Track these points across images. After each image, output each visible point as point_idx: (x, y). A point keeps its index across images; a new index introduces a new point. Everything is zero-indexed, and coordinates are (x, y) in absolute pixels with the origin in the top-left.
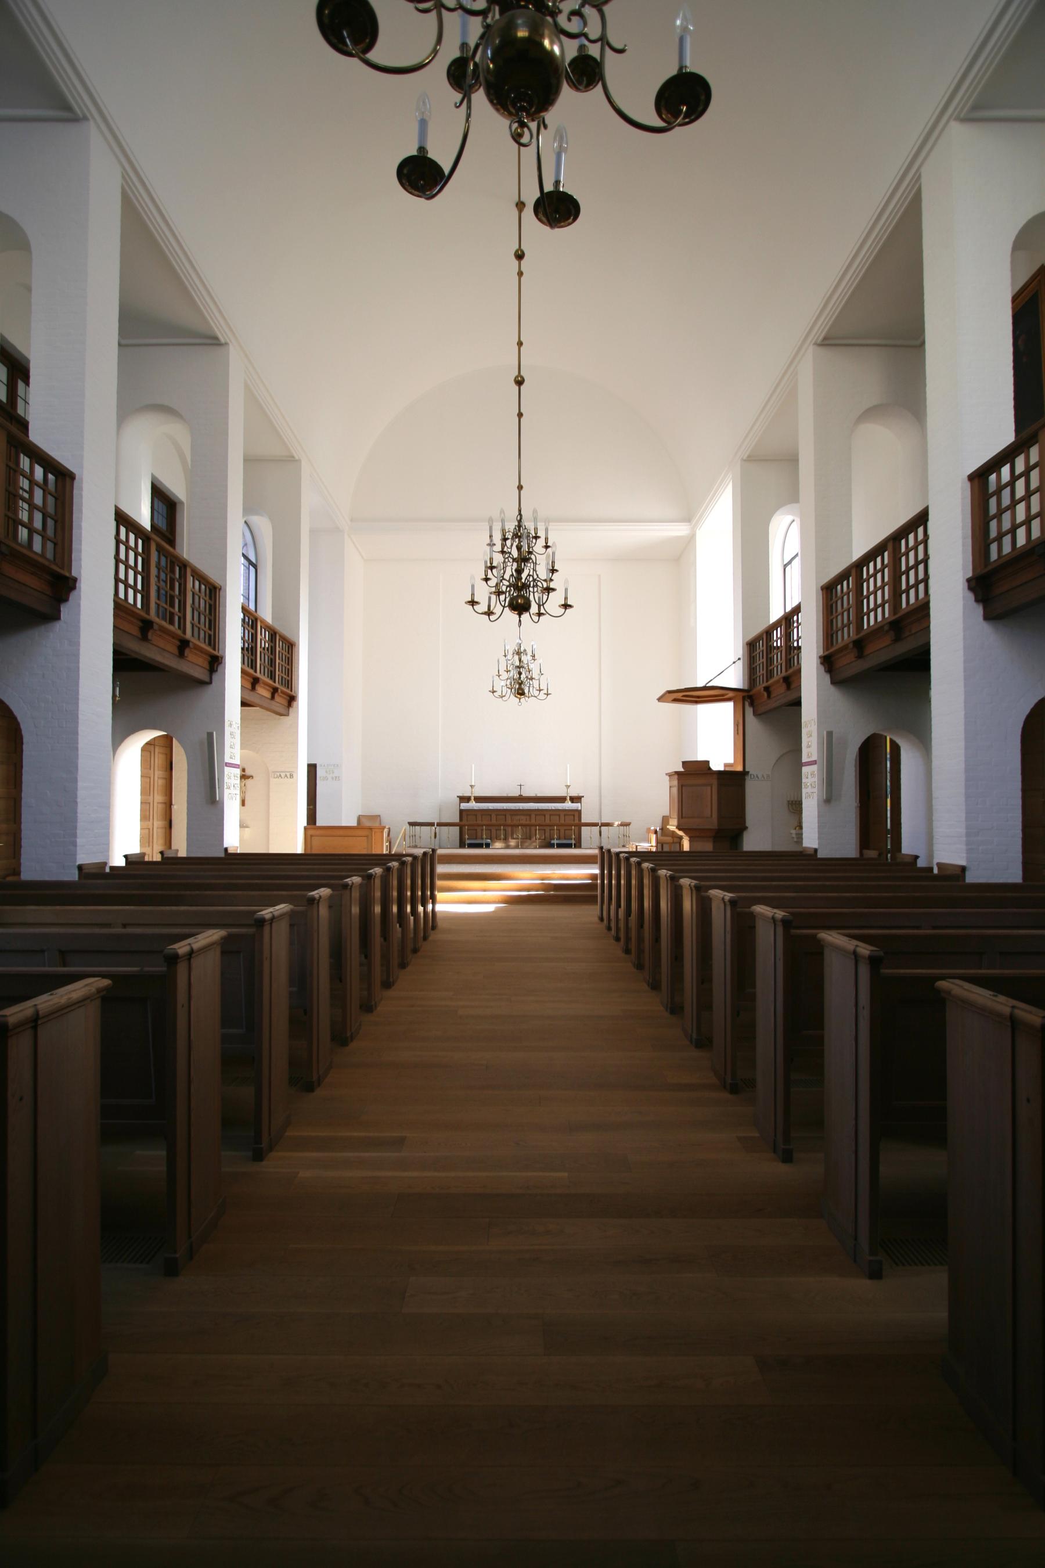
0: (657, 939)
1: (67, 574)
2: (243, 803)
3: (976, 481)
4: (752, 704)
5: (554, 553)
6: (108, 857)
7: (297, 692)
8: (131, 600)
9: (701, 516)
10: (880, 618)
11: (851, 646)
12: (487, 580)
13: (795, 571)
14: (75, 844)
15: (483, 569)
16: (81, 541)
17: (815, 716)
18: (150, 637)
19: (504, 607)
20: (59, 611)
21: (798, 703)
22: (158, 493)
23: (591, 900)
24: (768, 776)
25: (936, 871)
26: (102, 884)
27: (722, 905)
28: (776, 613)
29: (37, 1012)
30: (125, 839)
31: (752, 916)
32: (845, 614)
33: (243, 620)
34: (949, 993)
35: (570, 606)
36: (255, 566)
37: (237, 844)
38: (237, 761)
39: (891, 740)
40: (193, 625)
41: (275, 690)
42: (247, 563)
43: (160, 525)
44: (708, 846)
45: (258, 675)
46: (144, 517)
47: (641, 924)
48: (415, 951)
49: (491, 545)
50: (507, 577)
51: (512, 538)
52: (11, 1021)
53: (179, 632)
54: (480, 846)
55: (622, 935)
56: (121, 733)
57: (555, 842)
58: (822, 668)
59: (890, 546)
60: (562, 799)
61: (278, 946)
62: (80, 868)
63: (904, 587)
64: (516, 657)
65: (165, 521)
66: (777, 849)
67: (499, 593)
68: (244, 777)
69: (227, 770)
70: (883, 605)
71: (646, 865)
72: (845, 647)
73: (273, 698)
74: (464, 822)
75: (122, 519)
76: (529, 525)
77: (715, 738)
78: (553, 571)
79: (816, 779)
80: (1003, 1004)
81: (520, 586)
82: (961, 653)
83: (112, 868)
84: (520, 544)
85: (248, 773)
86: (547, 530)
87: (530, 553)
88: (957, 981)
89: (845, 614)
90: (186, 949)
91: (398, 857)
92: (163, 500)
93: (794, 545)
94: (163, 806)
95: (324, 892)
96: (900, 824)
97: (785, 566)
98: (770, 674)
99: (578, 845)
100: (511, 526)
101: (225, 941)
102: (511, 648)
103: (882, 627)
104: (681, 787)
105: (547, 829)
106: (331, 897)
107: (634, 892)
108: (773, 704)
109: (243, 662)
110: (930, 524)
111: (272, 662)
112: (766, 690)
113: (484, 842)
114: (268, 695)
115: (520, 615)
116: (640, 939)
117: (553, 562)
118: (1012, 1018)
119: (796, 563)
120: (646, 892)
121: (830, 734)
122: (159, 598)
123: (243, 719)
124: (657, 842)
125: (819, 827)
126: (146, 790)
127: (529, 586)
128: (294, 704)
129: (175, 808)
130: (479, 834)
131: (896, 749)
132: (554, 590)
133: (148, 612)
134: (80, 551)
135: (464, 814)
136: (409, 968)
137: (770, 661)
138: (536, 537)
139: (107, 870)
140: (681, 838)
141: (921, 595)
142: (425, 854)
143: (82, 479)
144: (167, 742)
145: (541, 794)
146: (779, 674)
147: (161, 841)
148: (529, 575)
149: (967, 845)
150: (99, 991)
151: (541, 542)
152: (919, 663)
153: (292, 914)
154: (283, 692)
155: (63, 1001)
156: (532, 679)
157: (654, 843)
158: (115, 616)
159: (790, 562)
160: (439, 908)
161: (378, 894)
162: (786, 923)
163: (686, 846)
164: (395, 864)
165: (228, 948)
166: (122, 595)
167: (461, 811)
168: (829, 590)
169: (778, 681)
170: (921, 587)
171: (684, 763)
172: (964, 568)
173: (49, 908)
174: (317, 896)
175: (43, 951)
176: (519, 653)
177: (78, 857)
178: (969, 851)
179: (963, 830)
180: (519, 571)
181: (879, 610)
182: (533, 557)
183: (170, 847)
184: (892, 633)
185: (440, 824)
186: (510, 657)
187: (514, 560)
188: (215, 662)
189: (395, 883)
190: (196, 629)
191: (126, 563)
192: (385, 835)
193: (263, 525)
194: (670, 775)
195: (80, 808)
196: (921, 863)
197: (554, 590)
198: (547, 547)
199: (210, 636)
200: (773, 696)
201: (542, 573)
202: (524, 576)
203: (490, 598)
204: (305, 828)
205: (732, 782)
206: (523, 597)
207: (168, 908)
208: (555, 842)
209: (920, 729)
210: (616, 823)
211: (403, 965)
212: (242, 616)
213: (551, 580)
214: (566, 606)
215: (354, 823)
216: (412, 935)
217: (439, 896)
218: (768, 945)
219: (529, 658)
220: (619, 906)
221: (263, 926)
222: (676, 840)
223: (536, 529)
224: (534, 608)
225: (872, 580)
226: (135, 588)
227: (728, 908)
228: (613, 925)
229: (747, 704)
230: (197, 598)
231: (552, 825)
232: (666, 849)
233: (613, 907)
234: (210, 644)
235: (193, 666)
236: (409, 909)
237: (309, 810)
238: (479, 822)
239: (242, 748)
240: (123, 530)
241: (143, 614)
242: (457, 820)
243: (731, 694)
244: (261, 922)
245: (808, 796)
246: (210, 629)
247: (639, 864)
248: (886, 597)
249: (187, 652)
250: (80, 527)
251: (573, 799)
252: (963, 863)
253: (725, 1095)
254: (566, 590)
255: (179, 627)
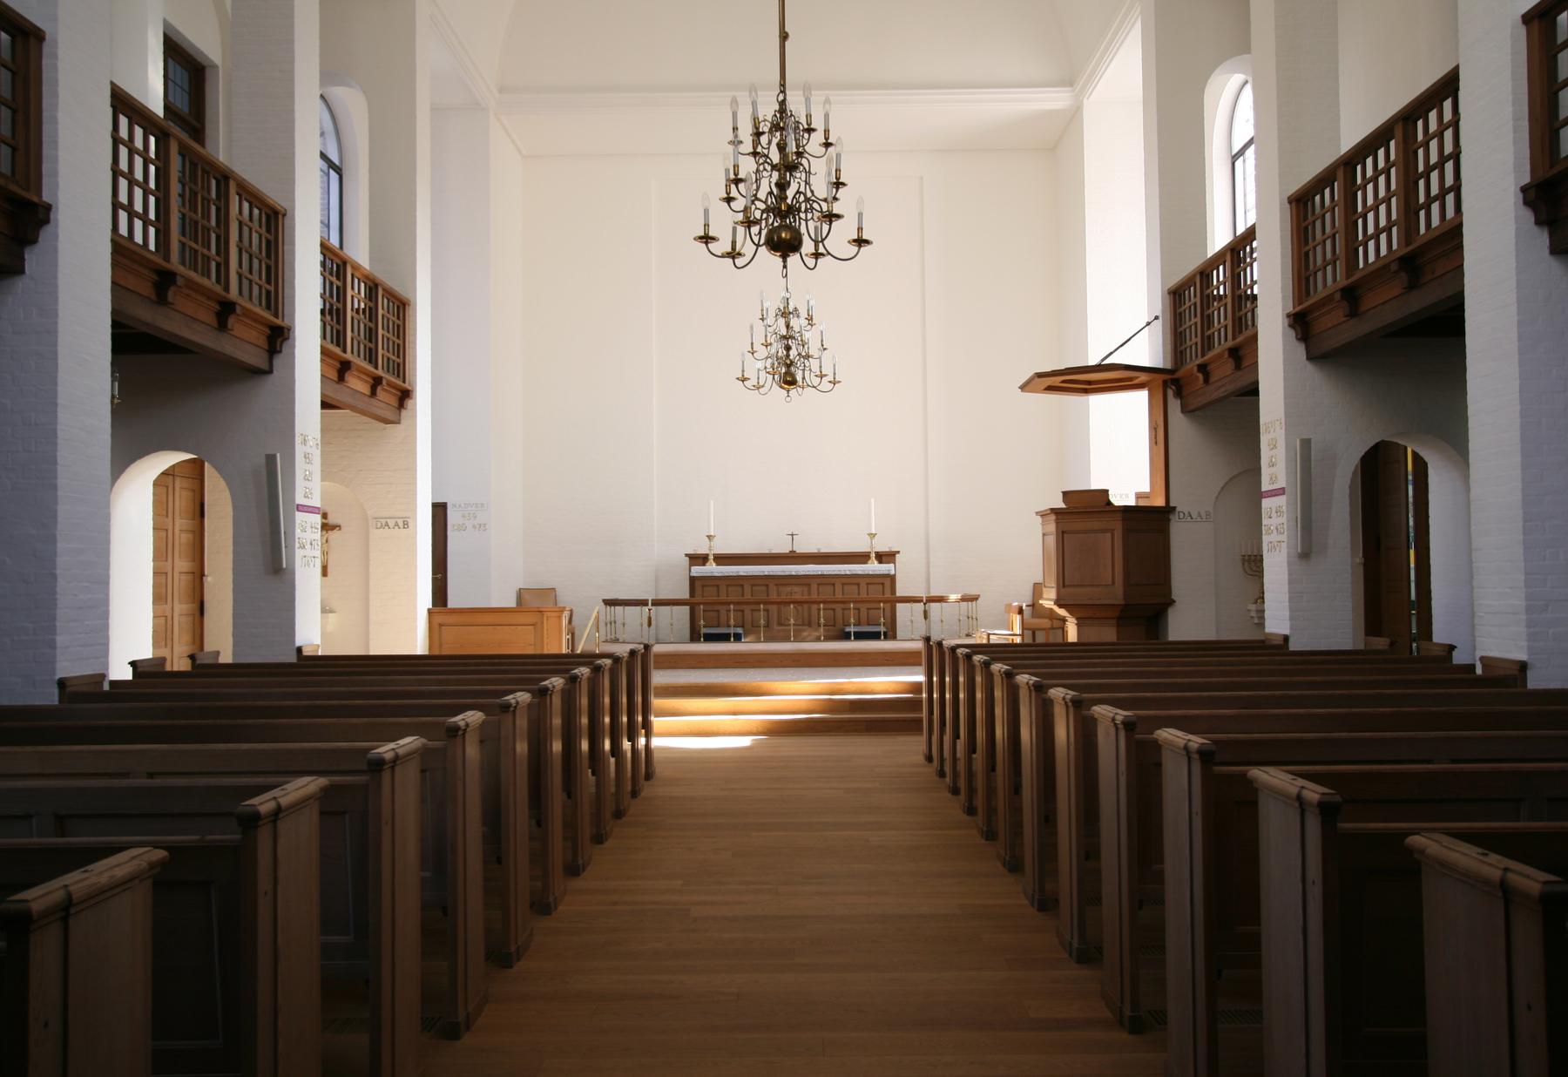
0: (1017, 789)
1: (35, 199)
2: (325, 573)
3: (1536, 23)
4: (1178, 394)
5: (838, 156)
6: (106, 665)
7: (414, 383)
8: (138, 238)
9: (1093, 73)
10: (1384, 251)
11: (1338, 296)
12: (729, 200)
13: (1248, 166)
14: (52, 645)
15: (724, 182)
16: (56, 143)
17: (1281, 413)
18: (170, 299)
19: (758, 245)
20: (23, 259)
21: (1253, 391)
22: (175, 51)
23: (912, 727)
24: (1208, 514)
25: (1479, 671)
26: (94, 709)
27: (1113, 730)
28: (1219, 238)
29: (69, 895)
30: (131, 638)
31: (1156, 746)
32: (1328, 242)
33: (323, 264)
34: (1422, 852)
35: (867, 242)
36: (339, 170)
37: (318, 641)
38: (316, 502)
39: (1415, 454)
40: (240, 276)
41: (376, 382)
42: (325, 166)
43: (179, 104)
44: (1108, 634)
45: (348, 356)
46: (153, 92)
47: (991, 767)
48: (619, 814)
49: (736, 142)
50: (762, 195)
51: (771, 131)
52: (36, 907)
53: (218, 289)
54: (724, 638)
55: (962, 784)
56: (125, 454)
57: (852, 629)
58: (1292, 333)
59: (1399, 131)
60: (862, 558)
61: (404, 804)
62: (62, 683)
63: (1422, 199)
64: (782, 321)
65: (186, 97)
66: (1225, 636)
67: (749, 223)
68: (326, 527)
69: (300, 517)
70: (1388, 229)
71: (997, 667)
72: (1329, 299)
73: (373, 393)
74: (698, 599)
75: (122, 103)
76: (796, 105)
77: (1118, 451)
78: (838, 184)
79: (1284, 519)
80: (1491, 865)
81: (783, 210)
82: (1514, 309)
83: (114, 684)
84: (784, 142)
85: (331, 520)
86: (827, 116)
87: (799, 154)
88: (1436, 836)
89: (1328, 242)
90: (271, 805)
91: (588, 658)
92: (184, 63)
93: (1245, 129)
94: (190, 577)
95: (473, 717)
96: (1429, 592)
97: (1235, 158)
98: (1208, 343)
99: (891, 634)
100: (768, 111)
101: (326, 792)
102: (773, 305)
103: (1386, 267)
104: (1062, 535)
105: (838, 607)
106: (483, 725)
107: (980, 713)
108: (1213, 393)
109: (324, 337)
110: (1461, 94)
111: (371, 334)
112: (1200, 373)
113: (732, 631)
114: (366, 389)
115: (784, 257)
116: (991, 791)
117: (838, 171)
118: (1503, 884)
119: (1250, 152)
120: (998, 711)
121: (1306, 444)
122: (183, 233)
123: (325, 429)
124: (1023, 628)
125: (1291, 599)
126: (162, 552)
127: (799, 210)
128: (409, 403)
129: (209, 580)
130: (723, 618)
131: (1421, 466)
132: (838, 216)
133: (167, 258)
134: (55, 160)
135: (698, 584)
136: (608, 844)
137: (1207, 321)
138: (810, 130)
139: (106, 687)
140: (1064, 620)
141: (1450, 213)
142: (633, 653)
143: (55, 41)
144: (195, 471)
145: (825, 550)
146: (1220, 346)
147: (187, 638)
148: (798, 192)
149: (1528, 626)
150: (152, 866)
151: (818, 137)
152: (1448, 323)
153: (424, 753)
154: (390, 384)
155: (104, 879)
156: (808, 357)
157: (1017, 630)
158: (115, 265)
159: (1242, 152)
160: (656, 742)
161: (557, 721)
162: (1206, 756)
163: (1072, 634)
164: (584, 671)
165: (330, 805)
166: (123, 230)
167: (693, 580)
168: (1301, 203)
169: (1220, 356)
170: (1450, 198)
171: (1065, 494)
172: (1517, 167)
173: (29, 749)
174: (462, 724)
175: (28, 817)
176: (785, 314)
177: (59, 665)
178: (1531, 637)
179: (1519, 602)
180: (782, 186)
181: (1383, 237)
182: (804, 161)
183: (202, 648)
184: (1403, 275)
185: (657, 603)
186: (770, 321)
187: (774, 167)
188: (278, 337)
189: (585, 702)
190: (246, 283)
191: (130, 177)
192: (565, 622)
193: (352, 102)
194: (1043, 515)
195: (62, 585)
196: (1459, 658)
197: (838, 216)
198: (827, 145)
199: (268, 293)
200: (1214, 378)
201: (820, 188)
202: (790, 193)
203: (734, 230)
204: (430, 612)
205: (1147, 525)
206: (789, 228)
207: (221, 746)
208: (852, 629)
209: (1451, 430)
210: (953, 597)
211: (599, 839)
212: (319, 257)
213: (835, 199)
214: (860, 242)
215: (512, 603)
216: (613, 790)
217: (657, 722)
218: (1180, 789)
219: (804, 322)
220: (956, 736)
221: (381, 771)
222: (1057, 623)
223: (809, 116)
224: (808, 246)
225: (1370, 187)
226: (144, 217)
227: (1122, 734)
228: (948, 769)
229: (1170, 393)
230: (246, 230)
231: (832, 602)
232: (1040, 639)
233: (947, 738)
234: (268, 307)
235: (243, 344)
236: (607, 745)
237: (434, 580)
238: (723, 598)
239: (323, 480)
240: (123, 121)
241: (159, 260)
242: (686, 595)
243: (1143, 377)
244: (378, 765)
245: (1272, 548)
246: (268, 282)
247: (986, 665)
248: (1394, 217)
249: (231, 321)
250: (55, 121)
251: (882, 557)
252: (1522, 656)
253: (1124, 1036)
254: (860, 215)
255: (218, 281)
